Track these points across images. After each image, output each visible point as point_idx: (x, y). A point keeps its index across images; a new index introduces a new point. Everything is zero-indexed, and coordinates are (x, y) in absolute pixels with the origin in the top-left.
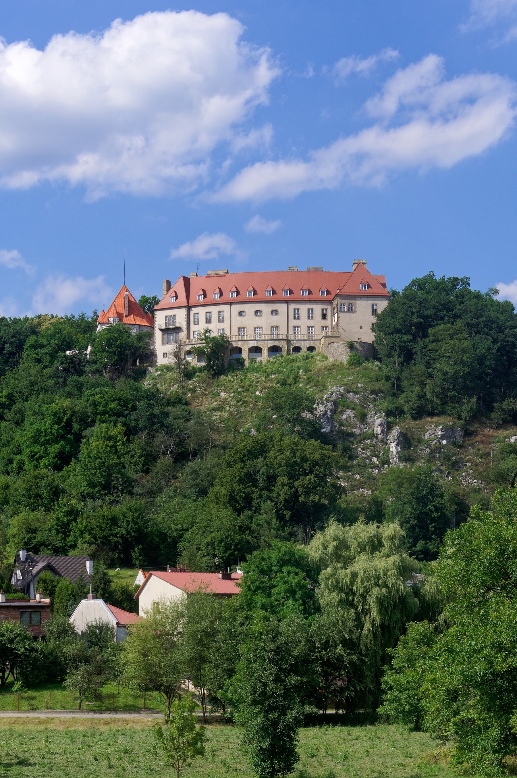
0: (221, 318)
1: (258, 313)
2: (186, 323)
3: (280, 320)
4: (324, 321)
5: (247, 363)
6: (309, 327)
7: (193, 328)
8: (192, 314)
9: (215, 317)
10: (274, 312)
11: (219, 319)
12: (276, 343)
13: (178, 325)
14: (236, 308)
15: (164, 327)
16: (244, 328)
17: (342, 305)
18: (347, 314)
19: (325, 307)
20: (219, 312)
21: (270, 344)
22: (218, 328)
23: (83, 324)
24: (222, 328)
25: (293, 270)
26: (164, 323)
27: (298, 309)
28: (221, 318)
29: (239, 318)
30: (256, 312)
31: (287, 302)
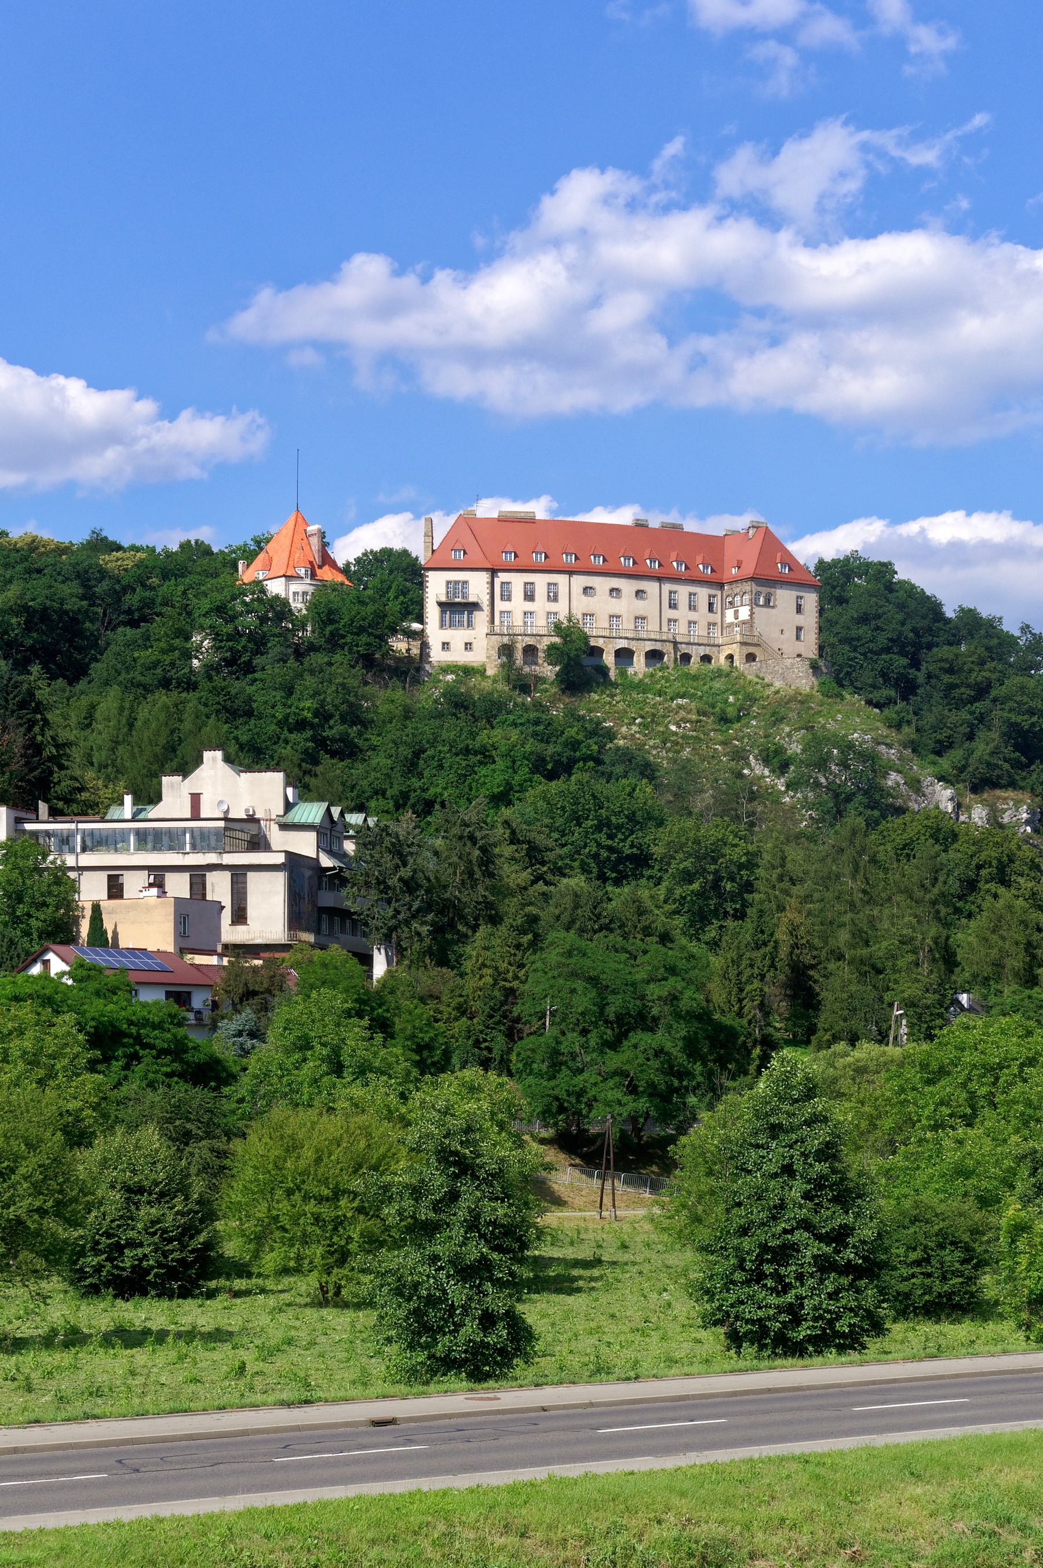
0: (552, 594)
1: (615, 592)
2: (488, 597)
3: (649, 607)
4: (693, 613)
5: (612, 674)
6: (690, 623)
7: (500, 606)
8: (497, 582)
9: (541, 592)
10: (640, 594)
11: (549, 596)
12: (658, 646)
13: (472, 599)
14: (580, 582)
15: (443, 599)
16: (592, 615)
17: (758, 594)
18: (765, 609)
19: (713, 592)
20: (549, 584)
21: (649, 646)
22: (548, 610)
23: (933, 813)
24: (554, 610)
25: (642, 525)
26: (444, 591)
27: (675, 592)
28: (552, 594)
29: (584, 598)
30: (612, 590)
31: (660, 579)
